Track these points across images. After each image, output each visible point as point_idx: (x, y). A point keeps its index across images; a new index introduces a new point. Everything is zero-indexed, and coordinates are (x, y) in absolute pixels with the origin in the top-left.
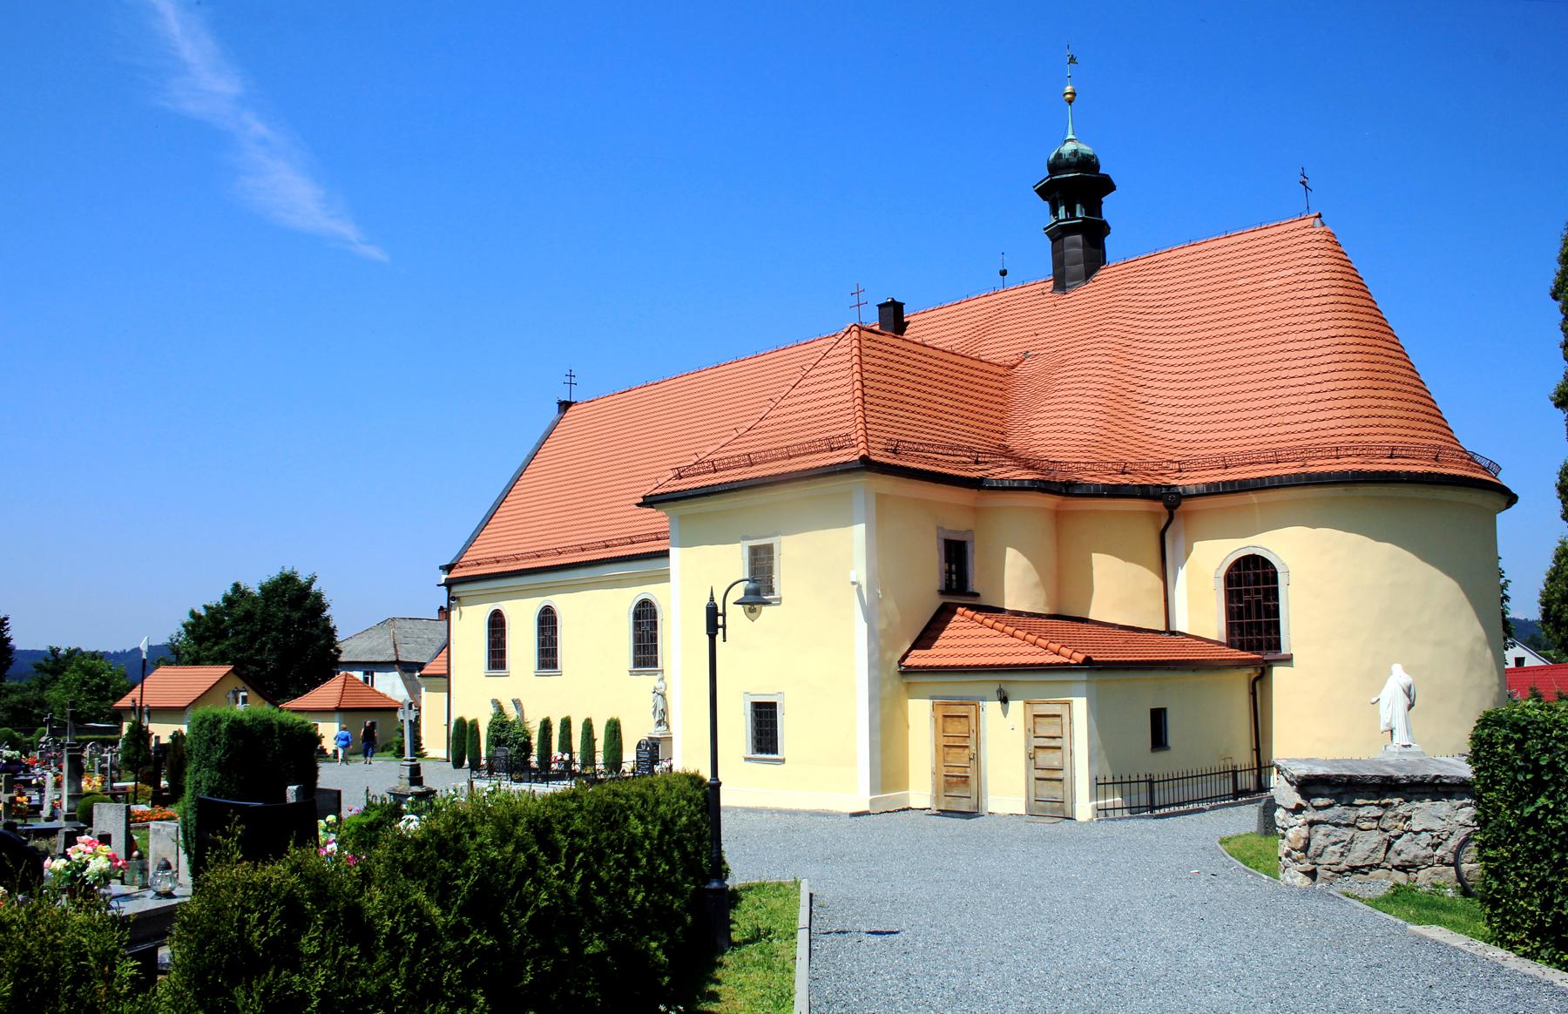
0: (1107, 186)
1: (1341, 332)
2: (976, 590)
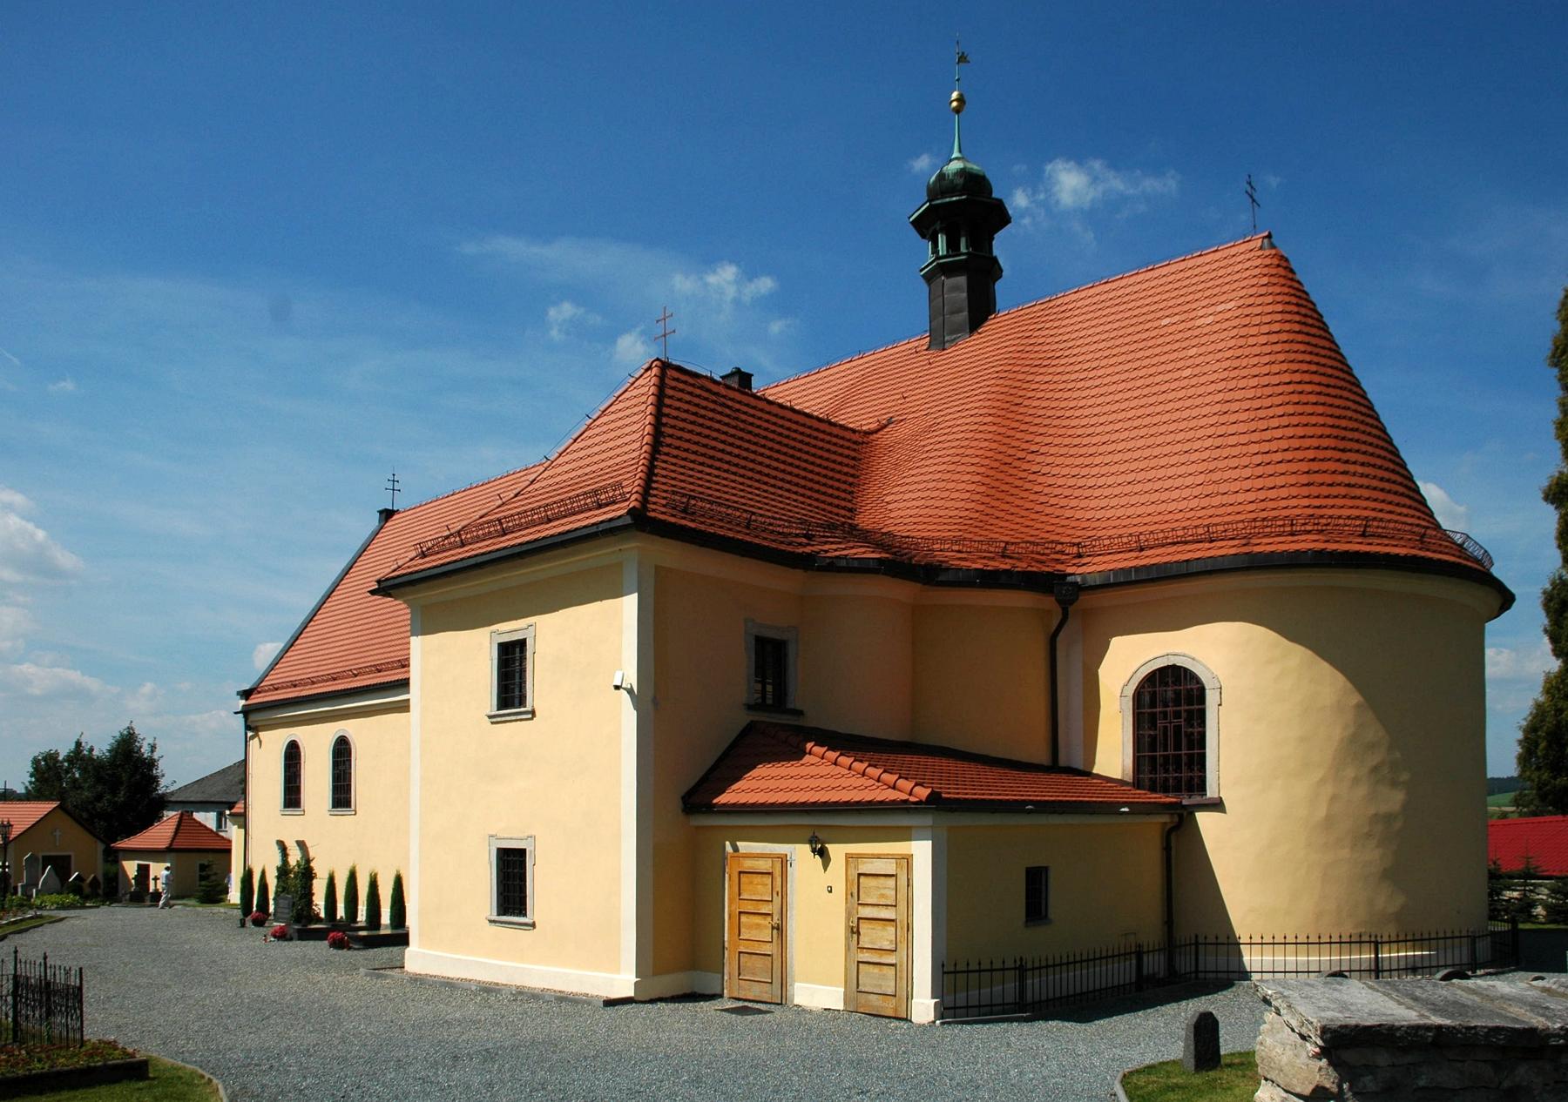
1: (1297, 377)
2: (799, 707)
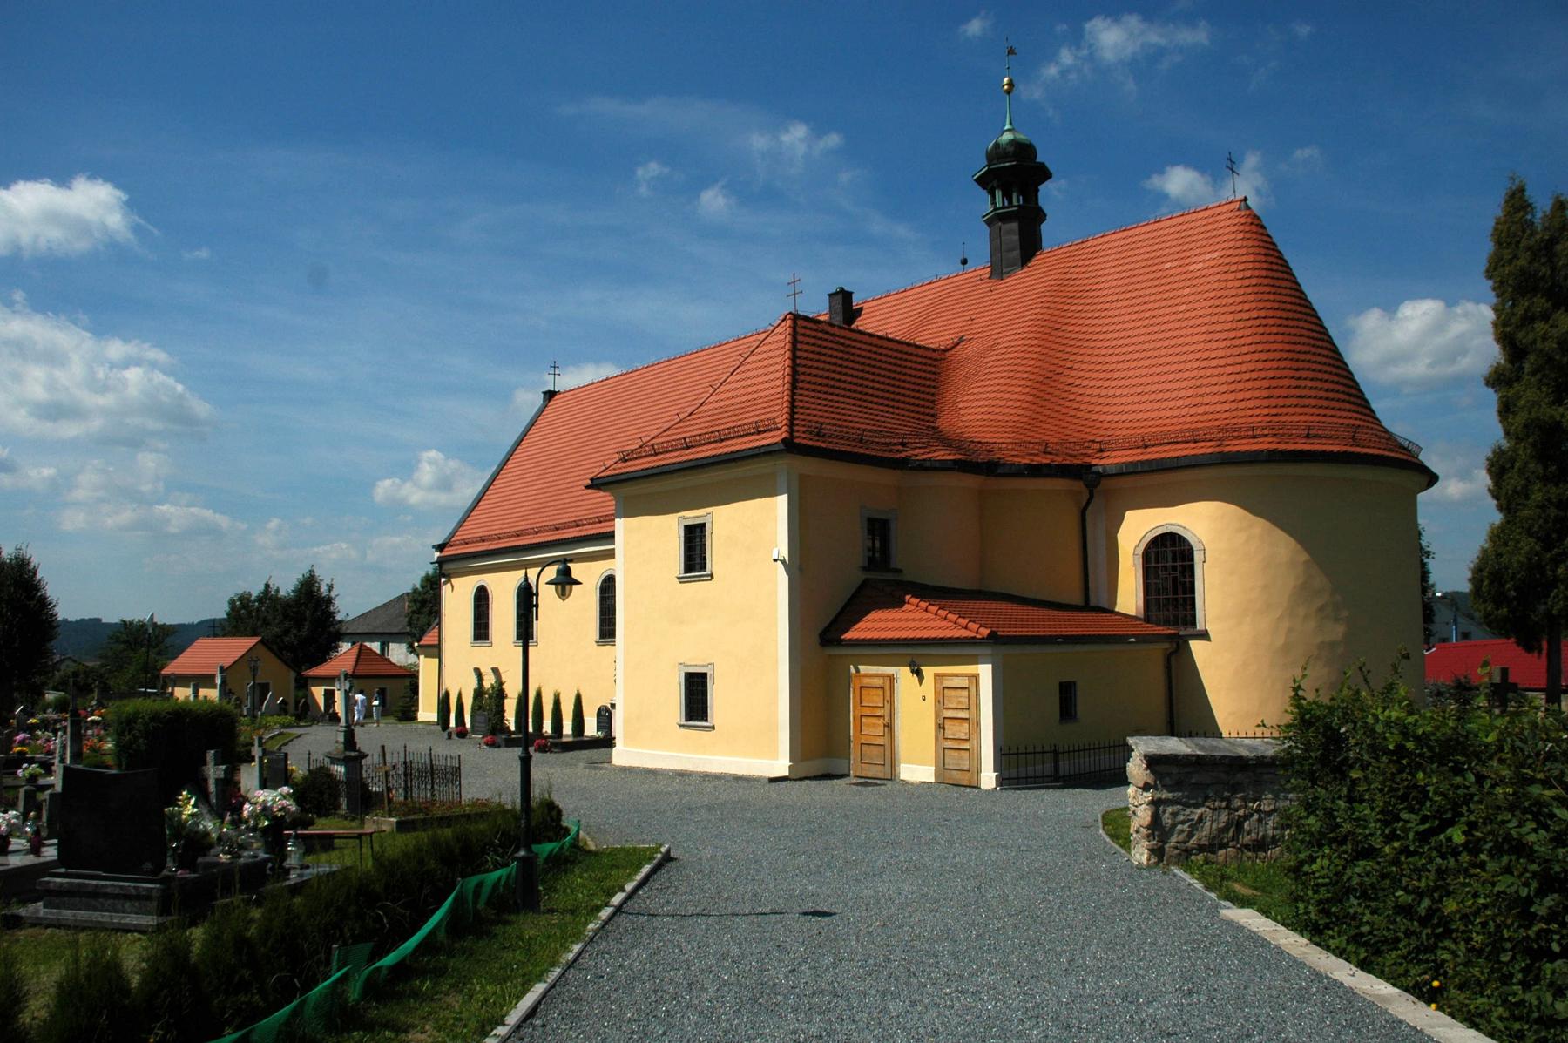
0: (1044, 174)
1: (1263, 313)
